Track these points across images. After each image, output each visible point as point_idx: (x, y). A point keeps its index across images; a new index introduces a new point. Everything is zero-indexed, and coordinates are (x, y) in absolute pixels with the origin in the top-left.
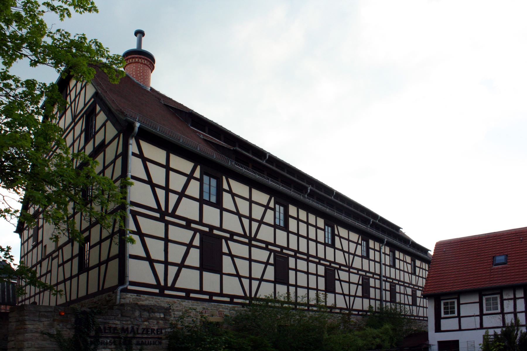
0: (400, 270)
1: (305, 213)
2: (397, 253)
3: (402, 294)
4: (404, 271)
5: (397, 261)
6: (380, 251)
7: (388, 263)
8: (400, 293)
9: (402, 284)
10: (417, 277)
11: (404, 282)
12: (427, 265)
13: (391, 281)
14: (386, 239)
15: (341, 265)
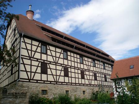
2: (106, 65)
5: (106, 67)
7: (103, 68)
11: (109, 74)
13: (94, 72)
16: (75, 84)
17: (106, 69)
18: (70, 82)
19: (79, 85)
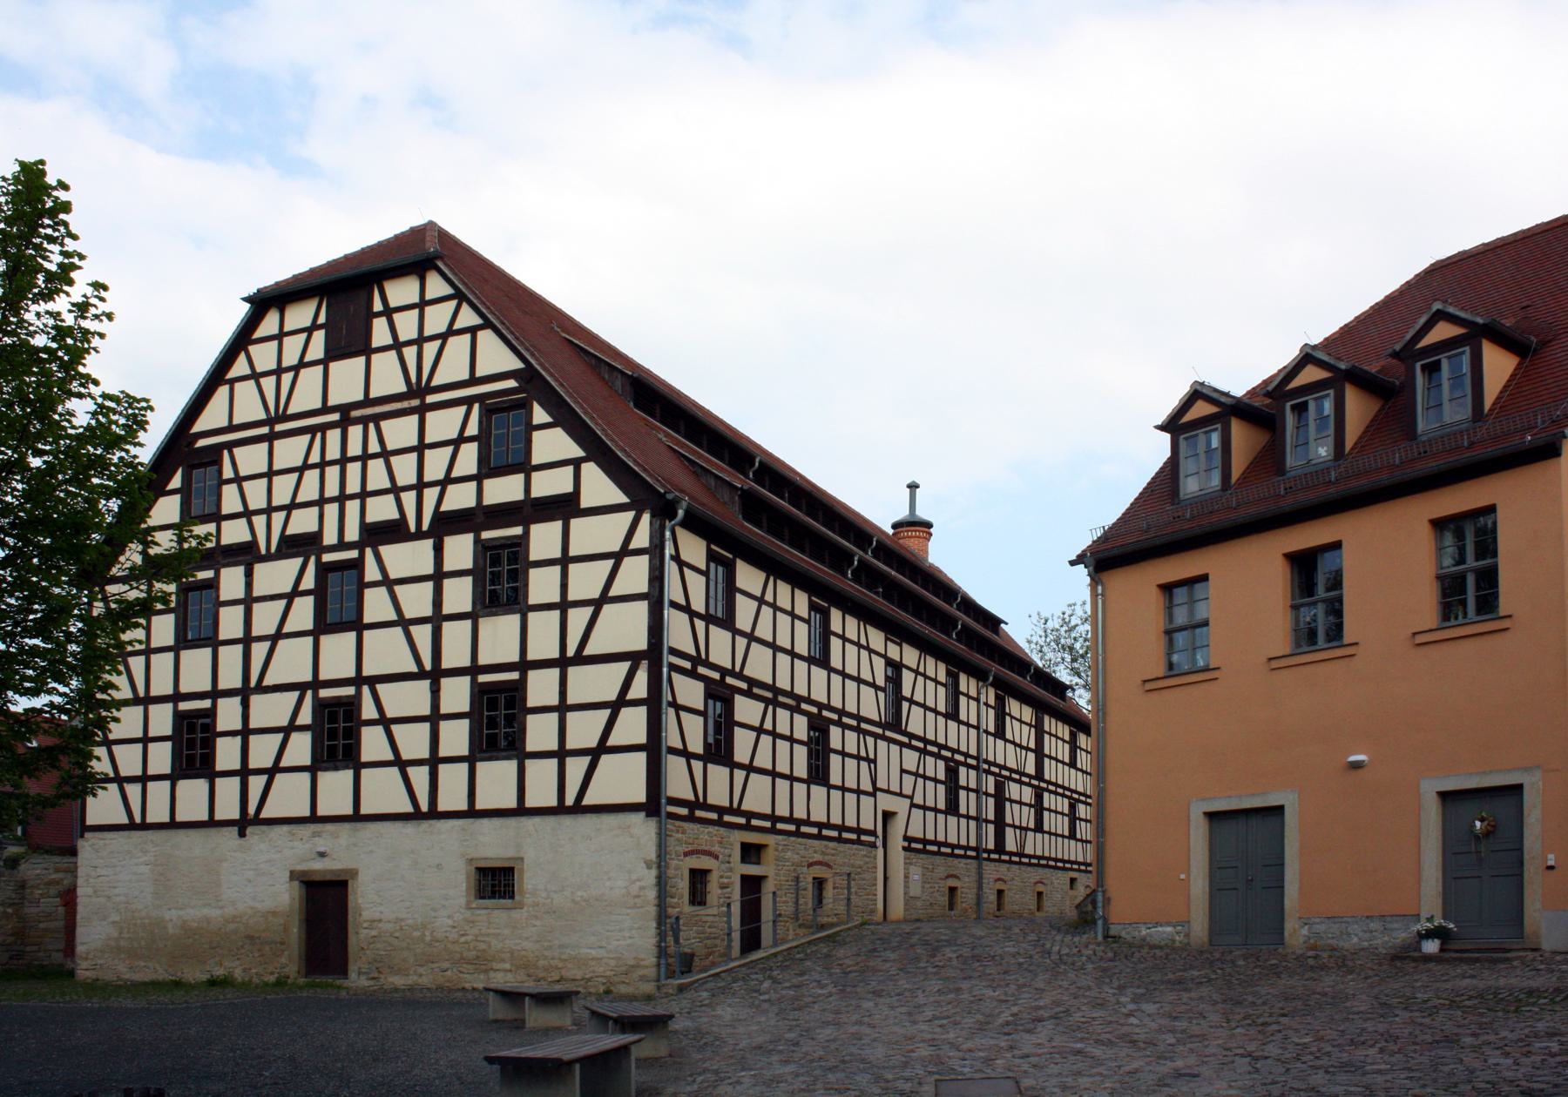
0: (844, 675)
1: (789, 587)
2: (836, 616)
3: (851, 756)
4: (858, 680)
5: (835, 644)
6: (977, 700)
7: (802, 648)
8: (843, 754)
9: (854, 723)
10: (741, 642)
11: (859, 718)
12: (942, 668)
13: (814, 710)
14: (995, 668)
15: (752, 682)
16: (768, 824)
17: (836, 662)
18: (833, 821)
19: (792, 828)
